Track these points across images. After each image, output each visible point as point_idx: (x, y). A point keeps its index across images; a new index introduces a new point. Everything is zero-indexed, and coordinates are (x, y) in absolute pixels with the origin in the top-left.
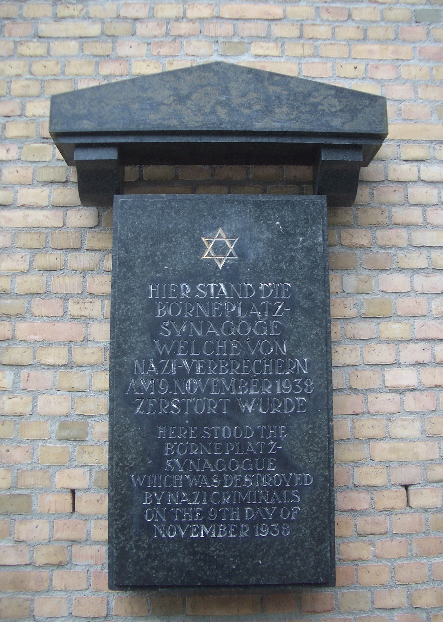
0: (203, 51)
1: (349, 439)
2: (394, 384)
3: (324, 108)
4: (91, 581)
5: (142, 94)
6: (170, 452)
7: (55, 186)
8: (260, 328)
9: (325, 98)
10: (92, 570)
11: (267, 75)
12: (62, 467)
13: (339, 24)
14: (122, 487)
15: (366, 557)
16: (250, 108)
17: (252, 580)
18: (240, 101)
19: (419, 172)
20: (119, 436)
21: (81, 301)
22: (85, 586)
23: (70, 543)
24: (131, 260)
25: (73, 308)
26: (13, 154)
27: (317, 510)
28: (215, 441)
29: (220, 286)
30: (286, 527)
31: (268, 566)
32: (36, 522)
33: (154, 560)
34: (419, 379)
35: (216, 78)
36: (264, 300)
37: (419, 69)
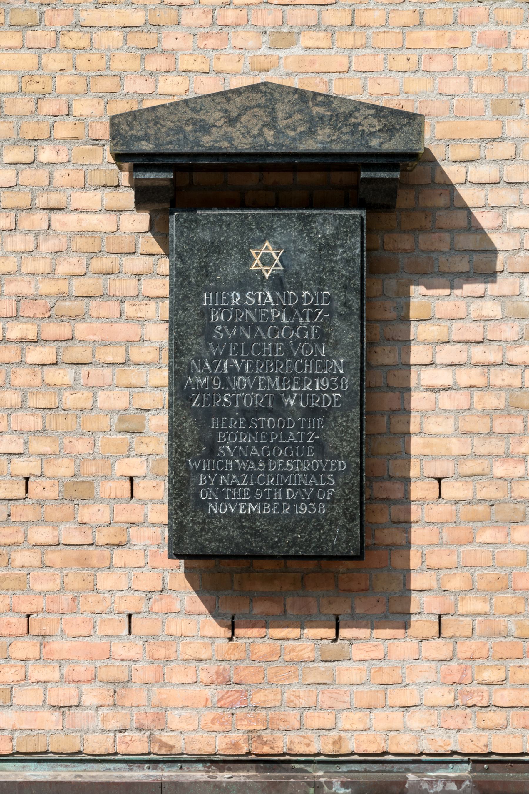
0: (251, 44)
1: (385, 433)
2: (430, 383)
3: (364, 128)
4: (148, 559)
5: (194, 116)
6: (222, 439)
7: (107, 189)
8: (302, 333)
9: (365, 118)
10: (148, 549)
11: (311, 96)
12: (122, 457)
13: (394, 8)
14: (180, 470)
15: (399, 542)
16: (294, 130)
17: (292, 552)
18: (284, 123)
19: (466, 173)
20: (178, 426)
21: (136, 303)
22: (143, 564)
23: (128, 525)
24: (187, 271)
25: (129, 310)
26: (63, 156)
27: (349, 492)
28: (261, 430)
29: (266, 295)
30: (321, 506)
31: (306, 539)
32: (97, 507)
33: (207, 533)
34: (454, 379)
35: (263, 100)
36: (307, 307)
37: (476, 58)
